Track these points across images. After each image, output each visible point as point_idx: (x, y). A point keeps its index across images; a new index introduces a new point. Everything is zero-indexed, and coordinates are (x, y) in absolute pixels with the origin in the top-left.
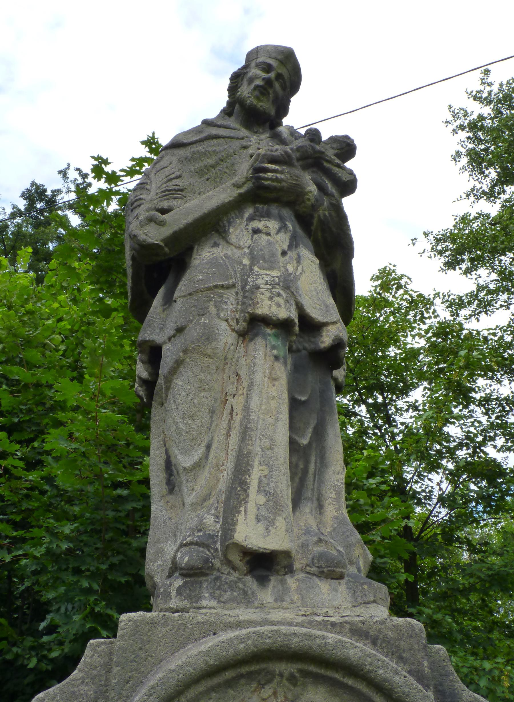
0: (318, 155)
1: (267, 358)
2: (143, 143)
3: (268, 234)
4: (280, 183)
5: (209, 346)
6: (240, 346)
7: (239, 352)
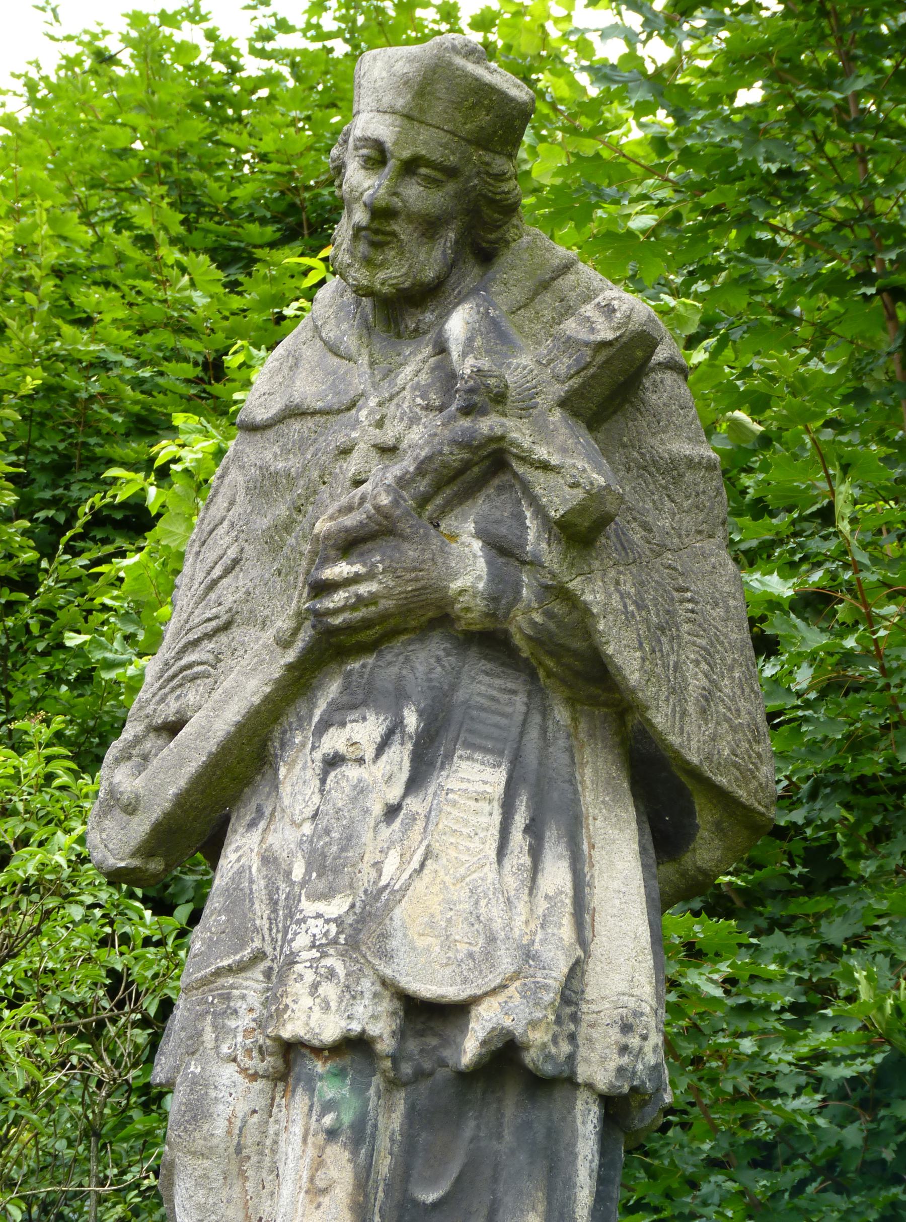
0: (494, 446)
1: (310, 1140)
3: (361, 761)
4: (375, 603)
5: (197, 1134)
6: (279, 1106)
7: (277, 1122)
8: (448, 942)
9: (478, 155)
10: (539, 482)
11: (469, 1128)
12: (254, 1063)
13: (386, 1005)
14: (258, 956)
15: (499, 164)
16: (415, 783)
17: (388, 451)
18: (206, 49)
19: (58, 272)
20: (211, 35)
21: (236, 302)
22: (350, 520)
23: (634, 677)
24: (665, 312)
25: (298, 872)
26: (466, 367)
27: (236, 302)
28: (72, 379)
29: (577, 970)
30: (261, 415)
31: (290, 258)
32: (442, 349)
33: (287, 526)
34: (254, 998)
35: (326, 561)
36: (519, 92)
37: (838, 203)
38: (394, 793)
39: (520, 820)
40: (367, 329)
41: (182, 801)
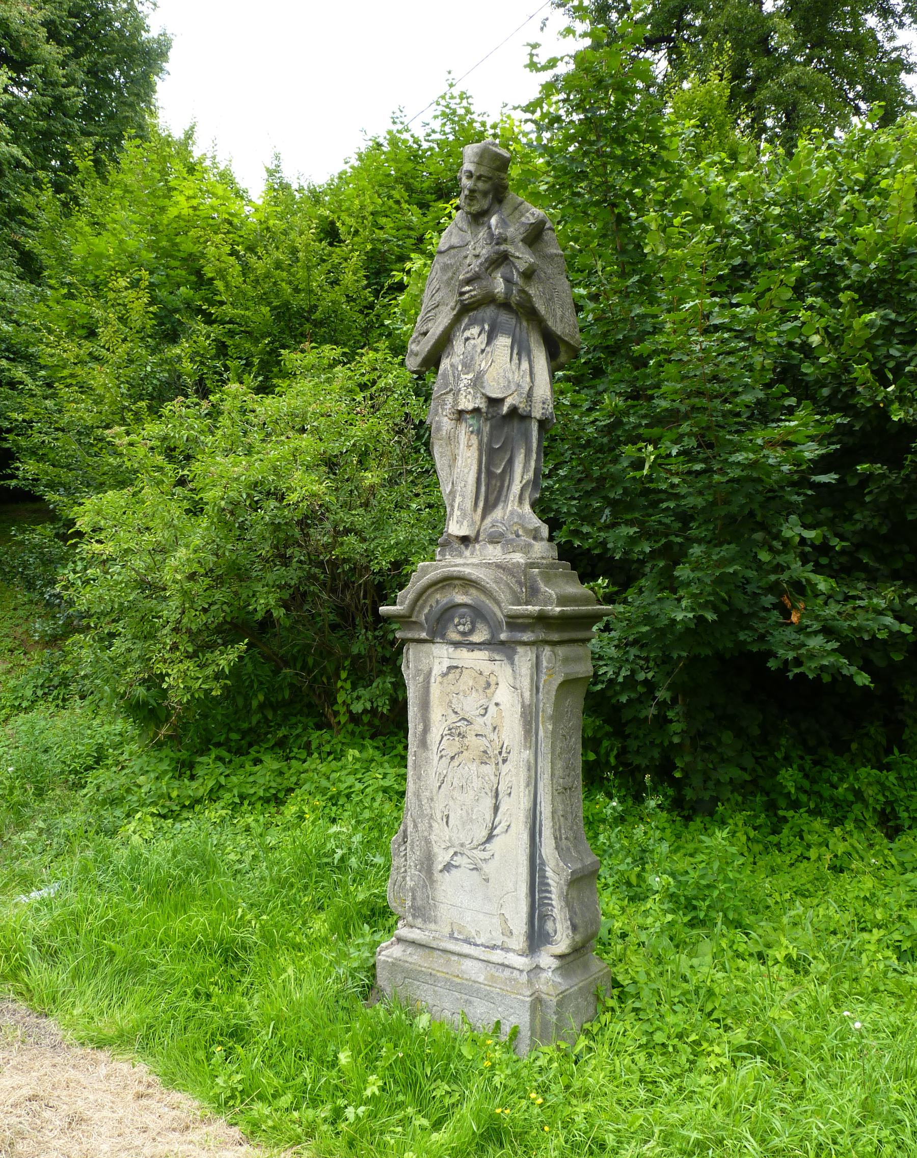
2: (526, 66)
8: (498, 383)
9: (497, 173)
10: (517, 262)
11: (506, 429)
12: (452, 416)
13: (484, 400)
14: (451, 390)
15: (503, 175)
16: (488, 344)
17: (477, 256)
18: (411, 140)
19: (372, 214)
20: (412, 136)
21: (425, 219)
22: (468, 275)
23: (543, 313)
24: (551, 214)
25: (460, 368)
26: (497, 232)
27: (425, 219)
28: (379, 246)
29: (531, 389)
30: (443, 249)
31: (441, 205)
32: (490, 228)
33: (452, 278)
34: (451, 400)
35: (463, 286)
36: (506, 154)
37: (598, 179)
38: (483, 346)
39: (515, 351)
40: (470, 223)
41: (429, 352)
